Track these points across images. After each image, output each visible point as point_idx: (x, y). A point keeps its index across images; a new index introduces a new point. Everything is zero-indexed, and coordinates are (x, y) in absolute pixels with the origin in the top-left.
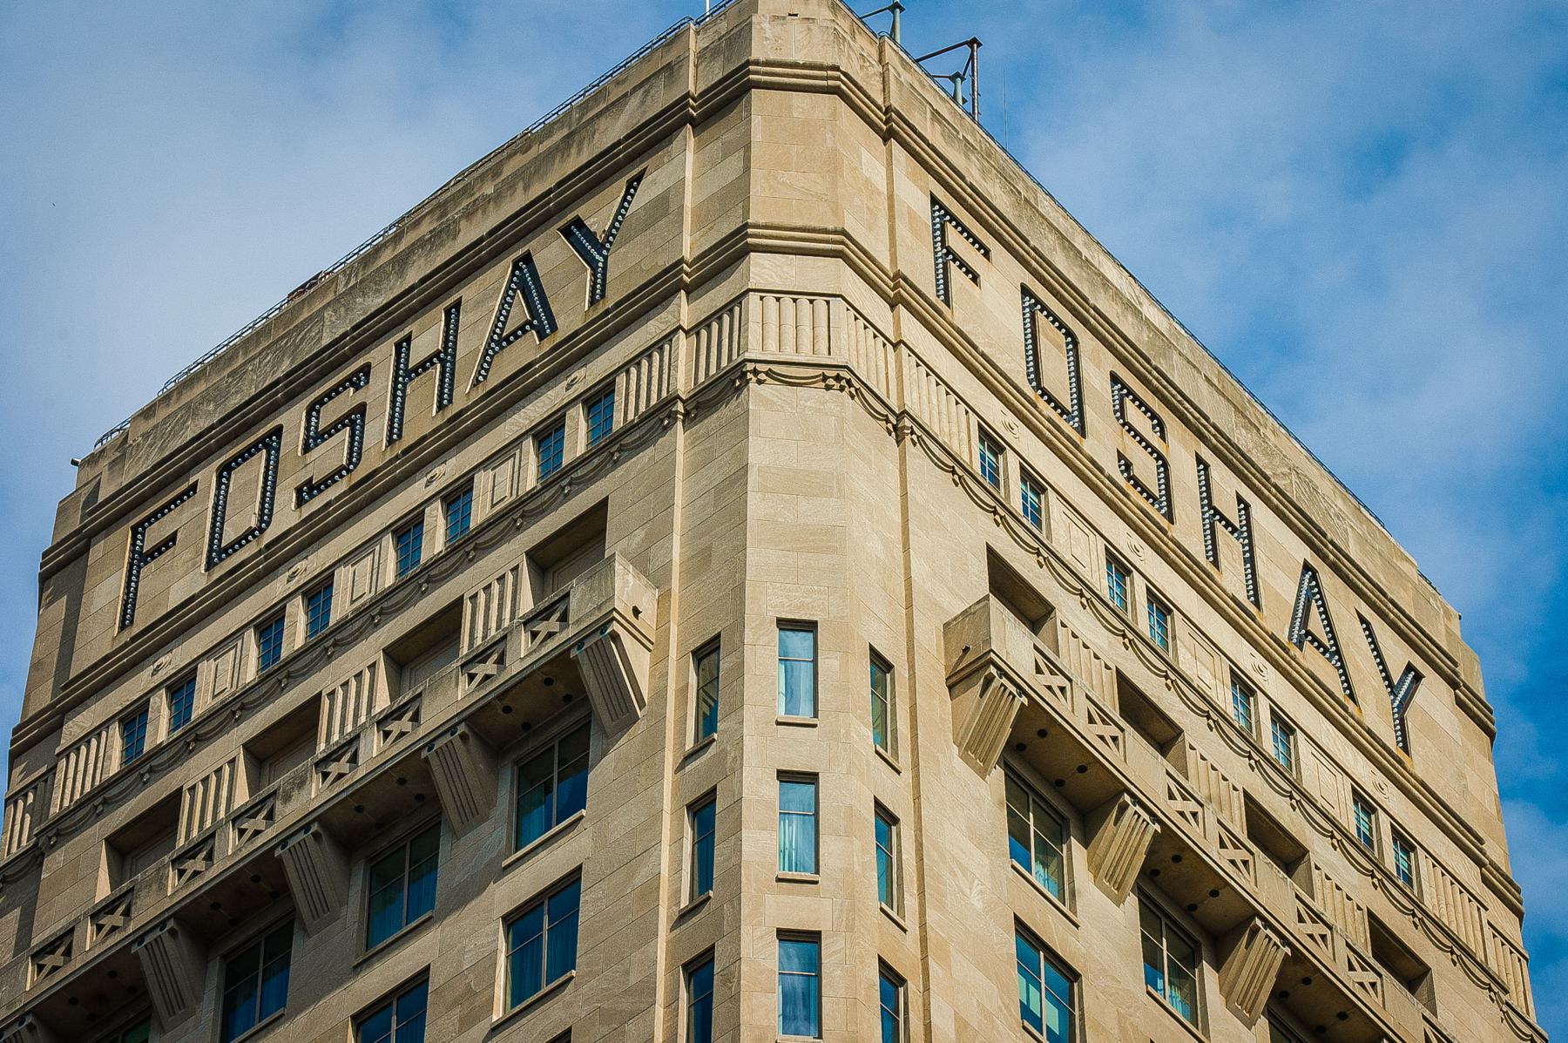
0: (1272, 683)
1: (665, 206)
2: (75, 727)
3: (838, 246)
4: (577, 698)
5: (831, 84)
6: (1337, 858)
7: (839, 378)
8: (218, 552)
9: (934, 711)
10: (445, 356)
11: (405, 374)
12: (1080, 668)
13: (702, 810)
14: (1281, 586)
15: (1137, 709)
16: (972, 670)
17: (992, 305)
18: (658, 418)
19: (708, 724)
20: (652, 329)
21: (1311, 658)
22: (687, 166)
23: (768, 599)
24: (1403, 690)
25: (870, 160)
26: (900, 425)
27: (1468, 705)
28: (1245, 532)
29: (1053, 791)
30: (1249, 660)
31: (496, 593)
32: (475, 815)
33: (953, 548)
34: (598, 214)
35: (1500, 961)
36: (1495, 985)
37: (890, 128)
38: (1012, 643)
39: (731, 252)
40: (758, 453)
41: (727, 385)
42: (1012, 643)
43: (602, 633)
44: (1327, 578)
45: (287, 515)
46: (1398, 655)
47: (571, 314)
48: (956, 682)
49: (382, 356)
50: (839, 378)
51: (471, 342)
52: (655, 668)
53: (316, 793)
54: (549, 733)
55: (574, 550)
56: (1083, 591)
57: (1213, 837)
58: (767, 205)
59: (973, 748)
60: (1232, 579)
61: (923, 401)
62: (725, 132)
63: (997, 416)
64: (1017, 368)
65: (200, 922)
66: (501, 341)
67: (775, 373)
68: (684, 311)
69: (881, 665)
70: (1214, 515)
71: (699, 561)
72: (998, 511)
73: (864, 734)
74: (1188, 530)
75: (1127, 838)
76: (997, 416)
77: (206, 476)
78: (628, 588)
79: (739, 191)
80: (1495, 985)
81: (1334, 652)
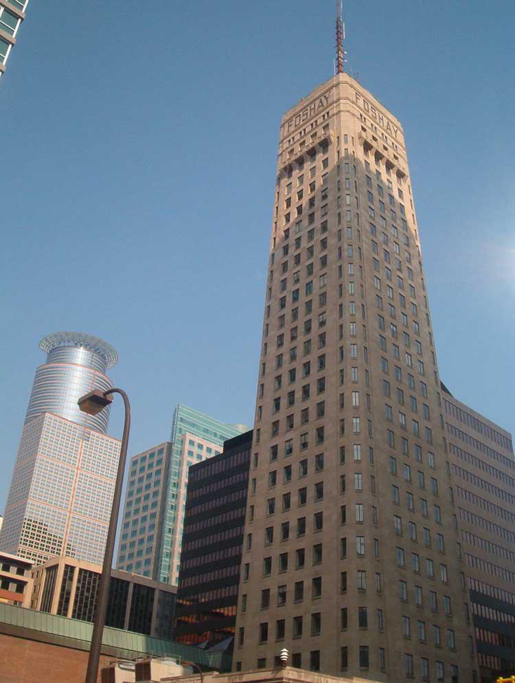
0: (385, 134)
1: (333, 95)
2: (284, 141)
3: (347, 99)
4: (327, 142)
5: (346, 83)
6: (229, 643)
7: (348, 111)
8: (296, 126)
9: (357, 141)
10: (314, 108)
11: (311, 110)
12: (368, 136)
13: (338, 152)
14: (386, 124)
15: (374, 138)
16: (360, 137)
17: (361, 102)
18: (333, 115)
19: (338, 145)
20: (332, 106)
21: (389, 131)
22: (334, 90)
23: (343, 134)
24: (396, 132)
25: (351, 90)
26: (354, 115)
27: (401, 132)
28: (382, 120)
29: (367, 147)
30: (383, 131)
31: (321, 132)
32: (319, 152)
33: (359, 124)
34: (327, 95)
35: (403, 155)
36: (404, 158)
37: (352, 86)
38: (364, 134)
39: (339, 100)
40: (342, 119)
41: (340, 112)
42: (364, 134)
43: (329, 136)
44: (390, 123)
45: (301, 123)
46: (396, 129)
47: (325, 105)
48: (359, 138)
49: (309, 108)
50: (348, 111)
51: (316, 108)
52: (333, 139)
53: (306, 150)
54: (325, 144)
55: (326, 127)
56: (369, 128)
57: (381, 150)
58: (341, 96)
59: (360, 145)
60: (382, 124)
61: (355, 112)
62: (338, 116)
63: (362, 112)
64: (362, 107)
65: (296, 161)
66: (319, 107)
67: (342, 111)
68: (335, 105)
69: (353, 138)
70: (380, 118)
71: (337, 129)
72: (362, 122)
73: (354, 190)
74: (378, 120)
75: (373, 151)
76: (362, 112)
77: (294, 118)
78: (331, 132)
79: (339, 94)
80: (404, 158)
81: (390, 130)
